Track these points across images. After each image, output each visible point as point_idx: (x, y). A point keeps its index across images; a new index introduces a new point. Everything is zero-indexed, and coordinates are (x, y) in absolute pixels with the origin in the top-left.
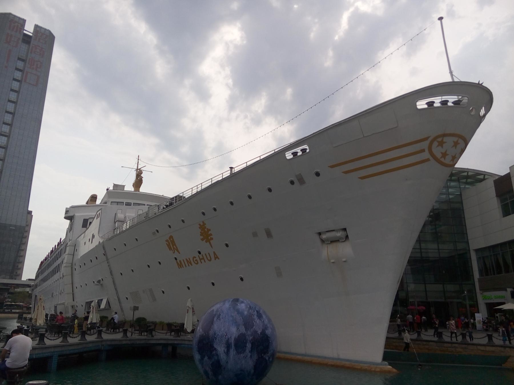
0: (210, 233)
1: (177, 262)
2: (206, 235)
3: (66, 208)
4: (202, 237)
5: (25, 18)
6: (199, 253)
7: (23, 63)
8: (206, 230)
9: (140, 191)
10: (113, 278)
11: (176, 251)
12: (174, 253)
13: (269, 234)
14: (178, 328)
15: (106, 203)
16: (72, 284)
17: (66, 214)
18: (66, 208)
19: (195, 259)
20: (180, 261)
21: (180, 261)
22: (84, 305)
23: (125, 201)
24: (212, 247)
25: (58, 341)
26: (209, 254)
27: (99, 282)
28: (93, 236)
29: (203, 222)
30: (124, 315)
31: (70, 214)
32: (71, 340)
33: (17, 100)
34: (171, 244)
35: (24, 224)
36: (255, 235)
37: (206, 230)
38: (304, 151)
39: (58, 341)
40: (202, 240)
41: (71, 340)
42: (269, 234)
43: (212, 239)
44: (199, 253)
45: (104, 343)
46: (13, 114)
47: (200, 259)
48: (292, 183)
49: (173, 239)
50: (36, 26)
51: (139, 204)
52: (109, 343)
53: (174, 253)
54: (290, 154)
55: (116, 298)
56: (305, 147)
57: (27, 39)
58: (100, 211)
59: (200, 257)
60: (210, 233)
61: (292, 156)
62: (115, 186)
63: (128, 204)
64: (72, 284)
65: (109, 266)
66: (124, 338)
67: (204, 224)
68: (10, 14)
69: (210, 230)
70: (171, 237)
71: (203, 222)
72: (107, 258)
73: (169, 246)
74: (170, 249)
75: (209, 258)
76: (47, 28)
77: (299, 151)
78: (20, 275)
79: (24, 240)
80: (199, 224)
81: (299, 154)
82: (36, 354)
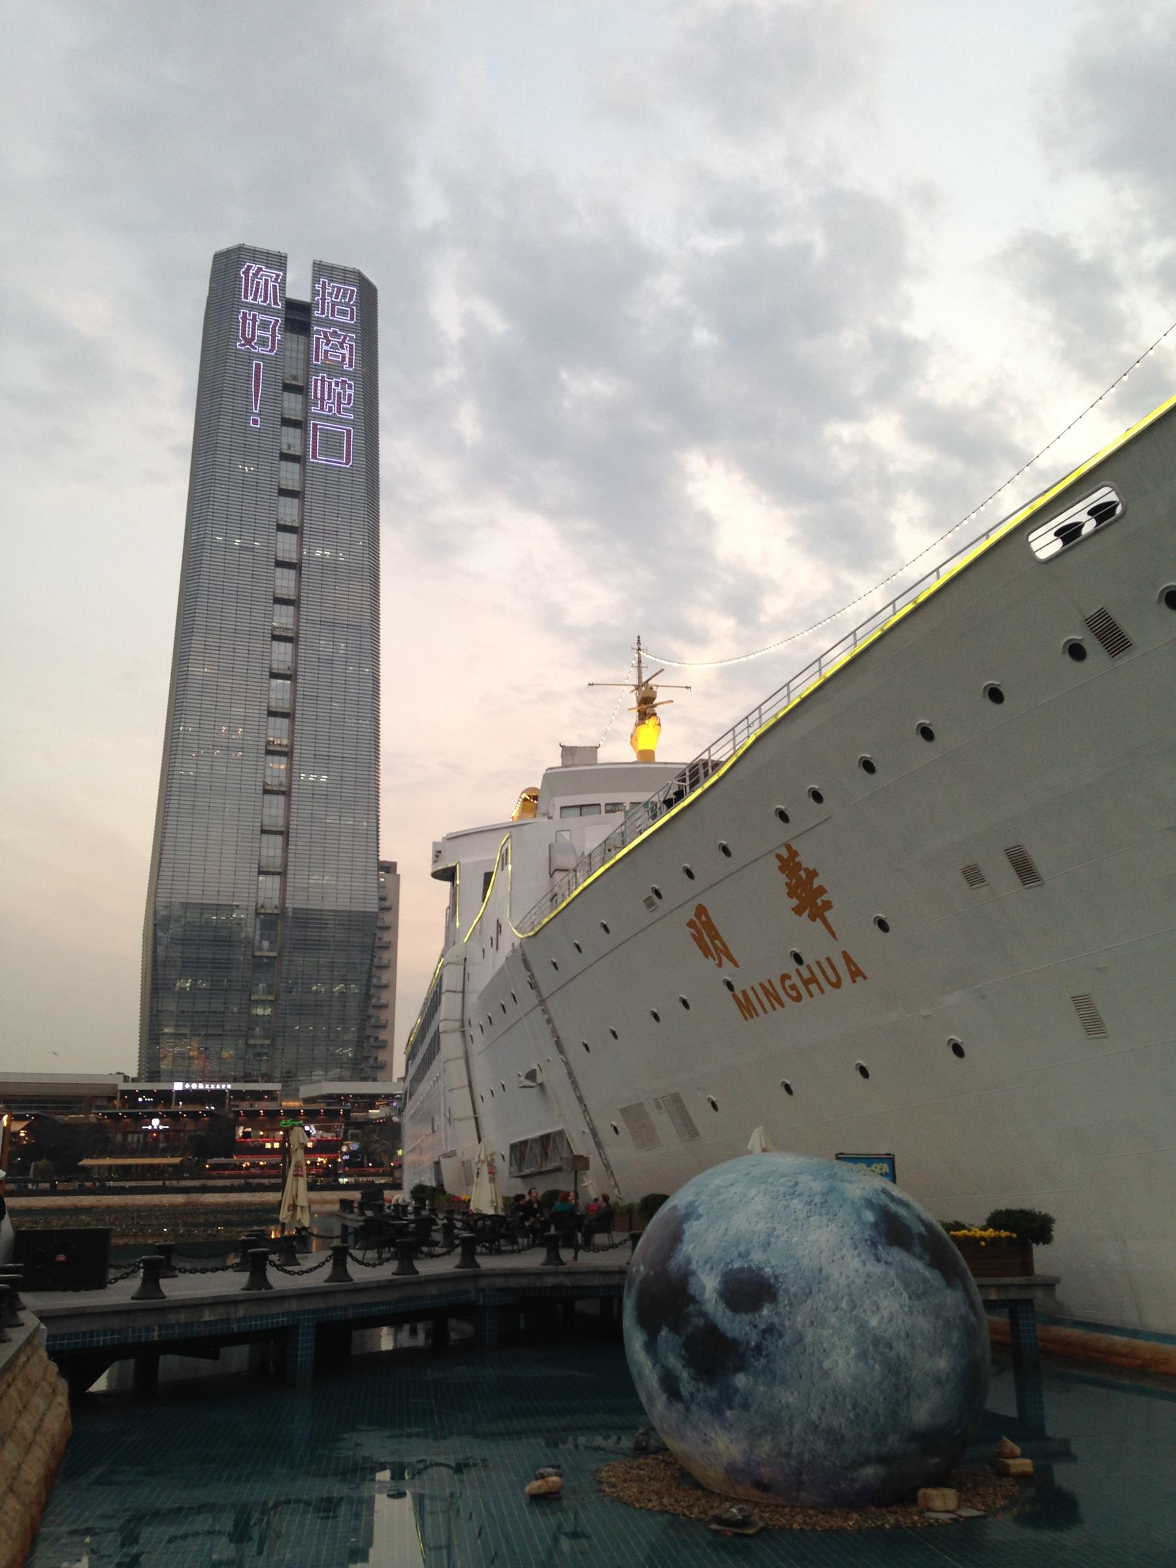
0: (817, 882)
1: (735, 996)
2: (808, 896)
3: (435, 844)
4: (794, 902)
6: (798, 958)
7: (300, 397)
8: (802, 873)
9: (657, 760)
10: (567, 1064)
11: (724, 958)
12: (720, 965)
13: (1024, 869)
14: (425, 1249)
16: (470, 1086)
17: (435, 862)
18: (435, 844)
19: (788, 983)
20: (744, 993)
22: (506, 1152)
23: (604, 798)
24: (833, 934)
25: (387, 1271)
26: (828, 959)
29: (788, 847)
32: (425, 1268)
34: (706, 934)
35: (373, 906)
36: (973, 876)
37: (802, 873)
38: (1102, 513)
39: (387, 1271)
40: (798, 911)
41: (425, 1268)
42: (1024, 869)
43: (828, 905)
44: (798, 958)
45: (483, 1283)
47: (806, 983)
48: (1076, 652)
49: (707, 916)
52: (500, 1282)
53: (720, 965)
54: (1051, 536)
56: (1104, 495)
59: (804, 979)
61: (1058, 545)
62: (568, 752)
64: (470, 1086)
65: (549, 1021)
66: (550, 1267)
67: (793, 854)
70: (701, 910)
71: (788, 847)
73: (699, 941)
75: (834, 979)
77: (1083, 517)
79: (385, 956)
80: (779, 857)
81: (1085, 531)
82: (239, 1320)
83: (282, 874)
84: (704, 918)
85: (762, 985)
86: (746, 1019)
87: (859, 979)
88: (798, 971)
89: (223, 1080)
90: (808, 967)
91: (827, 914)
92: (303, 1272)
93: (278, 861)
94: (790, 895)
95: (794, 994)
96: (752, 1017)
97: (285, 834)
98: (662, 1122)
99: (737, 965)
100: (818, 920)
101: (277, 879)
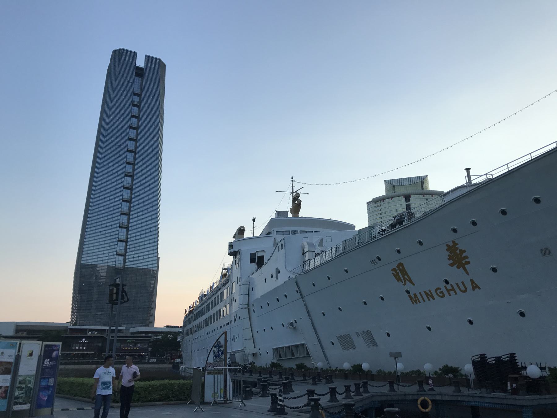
0: (464, 255)
2: (458, 258)
4: (451, 262)
5: (136, 51)
6: (447, 282)
8: (458, 252)
10: (311, 320)
15: (269, 233)
19: (439, 291)
20: (415, 295)
21: (415, 295)
22: (271, 352)
23: (291, 229)
26: (463, 283)
27: (292, 324)
28: (278, 272)
30: (328, 363)
31: (234, 249)
33: (137, 138)
34: (401, 273)
37: (458, 252)
40: (451, 265)
43: (468, 263)
44: (447, 282)
46: (134, 152)
47: (448, 291)
49: (403, 267)
50: (148, 58)
51: (306, 232)
52: (379, 399)
55: (317, 343)
57: (139, 72)
58: (283, 242)
60: (464, 255)
63: (295, 232)
65: (305, 305)
68: (122, 49)
69: (465, 251)
70: (400, 264)
72: (301, 295)
74: (399, 280)
75: (463, 289)
76: (157, 57)
78: (153, 322)
80: (447, 245)
83: (125, 255)
84: (401, 268)
85: (425, 292)
86: (413, 304)
87: (477, 290)
88: (445, 287)
89: (105, 326)
90: (451, 285)
91: (467, 266)
92: (291, 398)
93: (123, 251)
94: (449, 259)
95: (441, 295)
96: (416, 303)
97: (126, 242)
98: (360, 342)
99: (414, 284)
100: (461, 268)
101: (123, 257)
